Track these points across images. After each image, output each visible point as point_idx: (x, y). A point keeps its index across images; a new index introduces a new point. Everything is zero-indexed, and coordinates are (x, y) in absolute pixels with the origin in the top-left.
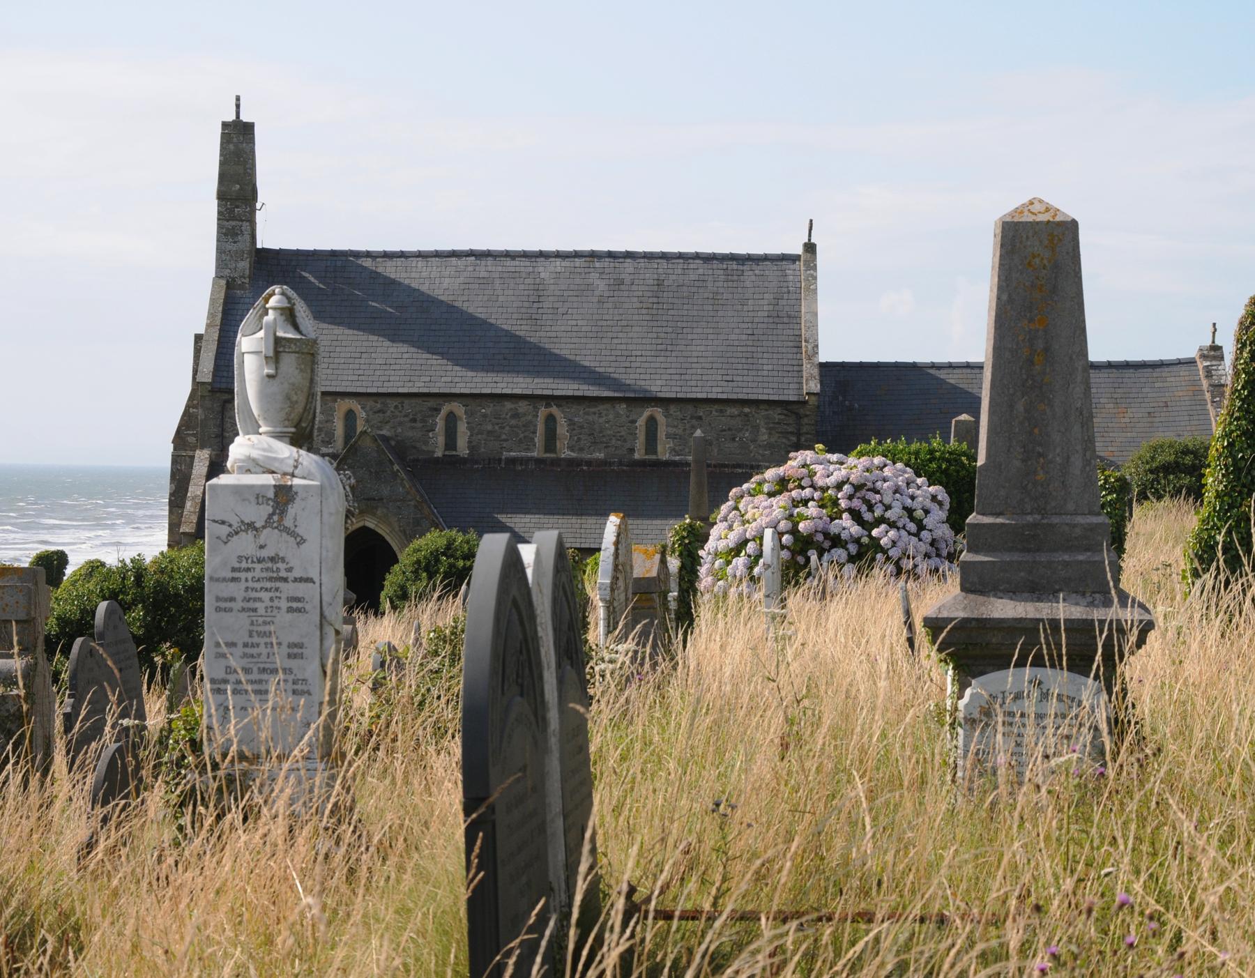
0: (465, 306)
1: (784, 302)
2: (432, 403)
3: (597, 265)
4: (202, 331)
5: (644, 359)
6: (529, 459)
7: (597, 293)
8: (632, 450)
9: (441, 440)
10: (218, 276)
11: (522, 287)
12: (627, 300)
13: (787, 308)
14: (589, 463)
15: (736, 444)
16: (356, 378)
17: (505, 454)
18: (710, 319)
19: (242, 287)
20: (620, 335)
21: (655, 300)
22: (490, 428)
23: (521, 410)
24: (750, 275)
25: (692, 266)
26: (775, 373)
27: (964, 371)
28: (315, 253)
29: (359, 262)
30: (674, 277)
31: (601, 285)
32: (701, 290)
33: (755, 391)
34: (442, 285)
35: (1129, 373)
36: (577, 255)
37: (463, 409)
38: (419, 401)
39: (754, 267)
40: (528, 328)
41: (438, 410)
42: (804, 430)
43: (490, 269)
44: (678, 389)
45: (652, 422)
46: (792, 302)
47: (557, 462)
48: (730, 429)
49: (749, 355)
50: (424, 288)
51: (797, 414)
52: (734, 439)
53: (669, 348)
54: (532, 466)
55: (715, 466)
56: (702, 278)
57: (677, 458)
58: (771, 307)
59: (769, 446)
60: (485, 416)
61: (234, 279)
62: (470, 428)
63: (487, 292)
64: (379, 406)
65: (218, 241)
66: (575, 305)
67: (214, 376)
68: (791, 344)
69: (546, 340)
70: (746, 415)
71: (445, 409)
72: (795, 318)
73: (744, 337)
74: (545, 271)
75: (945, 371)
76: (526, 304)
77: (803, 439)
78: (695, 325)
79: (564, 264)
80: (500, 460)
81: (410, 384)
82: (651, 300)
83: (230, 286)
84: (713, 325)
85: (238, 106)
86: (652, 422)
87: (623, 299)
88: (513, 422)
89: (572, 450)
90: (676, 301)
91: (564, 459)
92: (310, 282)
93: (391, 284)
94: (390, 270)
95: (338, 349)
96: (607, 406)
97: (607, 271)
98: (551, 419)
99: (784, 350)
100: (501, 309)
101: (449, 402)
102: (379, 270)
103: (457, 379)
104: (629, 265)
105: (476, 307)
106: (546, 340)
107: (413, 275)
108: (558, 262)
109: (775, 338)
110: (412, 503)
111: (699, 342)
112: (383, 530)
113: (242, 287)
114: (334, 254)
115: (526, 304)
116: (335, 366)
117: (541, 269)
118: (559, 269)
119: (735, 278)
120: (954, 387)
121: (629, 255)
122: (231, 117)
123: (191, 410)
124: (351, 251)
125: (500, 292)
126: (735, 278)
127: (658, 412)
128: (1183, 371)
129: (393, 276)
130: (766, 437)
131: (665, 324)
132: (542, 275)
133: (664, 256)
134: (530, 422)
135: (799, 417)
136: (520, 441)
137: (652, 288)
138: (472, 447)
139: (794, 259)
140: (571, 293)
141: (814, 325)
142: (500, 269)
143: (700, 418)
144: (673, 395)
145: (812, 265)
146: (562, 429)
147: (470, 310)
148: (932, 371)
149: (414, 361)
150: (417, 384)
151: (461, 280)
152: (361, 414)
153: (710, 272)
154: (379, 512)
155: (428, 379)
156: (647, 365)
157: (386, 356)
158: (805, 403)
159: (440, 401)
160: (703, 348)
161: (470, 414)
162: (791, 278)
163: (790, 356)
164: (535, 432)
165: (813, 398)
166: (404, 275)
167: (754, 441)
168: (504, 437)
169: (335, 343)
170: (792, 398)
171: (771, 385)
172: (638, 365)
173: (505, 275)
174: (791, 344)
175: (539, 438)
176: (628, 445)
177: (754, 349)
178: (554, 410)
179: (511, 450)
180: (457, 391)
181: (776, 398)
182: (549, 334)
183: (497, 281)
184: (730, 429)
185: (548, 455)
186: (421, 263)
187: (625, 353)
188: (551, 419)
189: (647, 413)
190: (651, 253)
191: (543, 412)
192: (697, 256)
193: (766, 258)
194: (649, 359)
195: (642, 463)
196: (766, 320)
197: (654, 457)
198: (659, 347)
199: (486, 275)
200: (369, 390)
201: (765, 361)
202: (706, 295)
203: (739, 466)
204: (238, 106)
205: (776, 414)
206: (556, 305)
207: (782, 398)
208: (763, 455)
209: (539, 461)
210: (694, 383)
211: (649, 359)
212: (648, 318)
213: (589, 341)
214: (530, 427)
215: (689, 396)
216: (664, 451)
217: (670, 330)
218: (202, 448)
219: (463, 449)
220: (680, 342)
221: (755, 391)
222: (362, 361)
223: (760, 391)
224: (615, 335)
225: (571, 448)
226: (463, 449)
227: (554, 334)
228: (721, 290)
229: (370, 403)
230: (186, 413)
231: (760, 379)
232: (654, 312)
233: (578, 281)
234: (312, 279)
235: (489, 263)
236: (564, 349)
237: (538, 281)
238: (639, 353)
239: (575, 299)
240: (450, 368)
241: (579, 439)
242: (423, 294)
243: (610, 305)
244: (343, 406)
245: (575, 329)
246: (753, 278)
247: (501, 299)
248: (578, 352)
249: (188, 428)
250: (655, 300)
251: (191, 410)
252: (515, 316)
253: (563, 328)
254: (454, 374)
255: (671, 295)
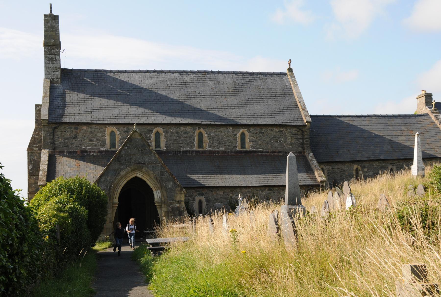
0: (156, 91)
1: (286, 89)
2: (149, 128)
3: (208, 76)
4: (40, 102)
5: (236, 110)
6: (192, 151)
7: (210, 86)
8: (235, 147)
9: (153, 144)
10: (46, 78)
11: (179, 83)
12: (223, 88)
13: (287, 92)
14: (218, 152)
15: (278, 143)
16: (114, 117)
17: (182, 149)
18: (258, 95)
19: (57, 82)
20: (224, 101)
21: (235, 88)
22: (175, 138)
23: (188, 131)
24: (270, 80)
25: (245, 76)
26: (291, 115)
27: (349, 118)
28: (88, 71)
29: (108, 74)
30: (240, 80)
31: (211, 83)
32: (252, 85)
33: (284, 121)
34: (146, 83)
35: (407, 118)
36: (199, 72)
37: (163, 130)
38: (143, 127)
39: (270, 77)
40: (185, 98)
41: (152, 131)
42: (305, 137)
43: (164, 77)
44: (254, 121)
45: (243, 135)
46: (289, 89)
47: (204, 152)
48: (275, 137)
49: (278, 108)
50: (137, 84)
51: (302, 131)
52: (277, 141)
53: (245, 106)
54: (194, 154)
55: (271, 153)
56: (251, 81)
57: (254, 150)
58: (281, 91)
59: (292, 144)
60: (172, 133)
61: (53, 79)
62: (166, 138)
63: (164, 85)
64: (125, 129)
65: (45, 63)
66: (202, 90)
67: (49, 117)
68: (294, 104)
69: (194, 103)
70: (282, 131)
71: (155, 130)
72: (291, 95)
73: (274, 102)
74: (187, 78)
75: (342, 118)
76: (182, 90)
77: (305, 141)
78: (253, 97)
79: (194, 75)
80: (180, 152)
81: (139, 120)
82: (233, 88)
83: (52, 82)
84: (260, 97)
85: (51, 8)
86: (243, 135)
87: (221, 88)
88: (185, 136)
89: (210, 147)
90: (243, 89)
91: (208, 151)
92: (87, 81)
93: (123, 83)
94: (121, 77)
95: (104, 106)
96: (224, 128)
97: (212, 78)
98: (200, 134)
99: (291, 106)
100: (173, 92)
101: (157, 127)
102: (117, 77)
103: (159, 118)
104: (221, 76)
105: (161, 91)
106: (194, 103)
107: (132, 79)
108: (192, 75)
109: (286, 102)
110: (160, 165)
111: (256, 104)
112: (145, 178)
113: (57, 82)
114: (96, 71)
115: (182, 90)
116: (104, 113)
117: (185, 77)
118: (192, 77)
119: (264, 81)
120: (348, 124)
121: (220, 72)
122: (48, 13)
123: (35, 136)
124: (104, 70)
125: (170, 85)
126: (264, 81)
127: (245, 131)
128: (426, 118)
129: (123, 79)
130: (290, 140)
131: (241, 97)
132: (186, 79)
133: (234, 73)
134: (192, 135)
135: (303, 132)
136: (188, 144)
137: (232, 84)
138: (167, 146)
139: (285, 74)
140: (200, 86)
141: (300, 97)
142: (168, 77)
143: (263, 133)
144: (252, 123)
145: (293, 76)
146: (206, 138)
147: (159, 92)
148: (338, 118)
149: (139, 111)
150: (142, 120)
151: (153, 81)
152: (117, 132)
153: (254, 79)
154: (144, 169)
155: (146, 118)
156: (238, 112)
157: (126, 109)
158: (306, 126)
159: (152, 127)
160: (259, 106)
161: (166, 132)
162: (286, 81)
163: (294, 109)
164: (194, 140)
165: (309, 124)
166: (127, 79)
167: (285, 142)
168: (181, 142)
169: (102, 104)
170: (300, 124)
171: (290, 119)
172: (234, 112)
173: (171, 79)
174: (294, 104)
175: (196, 142)
176: (234, 145)
177: (279, 106)
178: (202, 130)
179: (184, 148)
180: (160, 122)
181: (294, 124)
182: (194, 101)
183: (168, 81)
184: (275, 137)
185: (200, 149)
186: (134, 75)
187: (228, 108)
188: (200, 134)
189: (241, 131)
190: (229, 72)
191: (197, 131)
192: (247, 73)
193: (274, 74)
194: (238, 110)
195: (240, 152)
196: (281, 96)
197: (244, 149)
198: (241, 105)
199: (163, 79)
200: (121, 122)
201: (285, 111)
202: (254, 87)
203: (280, 152)
204: (51, 8)
205: (294, 131)
206: (194, 90)
207: (296, 124)
208: (289, 148)
209: (197, 152)
210: (259, 119)
211: (238, 110)
212: (233, 95)
213: (211, 103)
214: (192, 137)
215: (259, 123)
216: (248, 147)
217: (244, 99)
218: (44, 149)
219: (163, 147)
220: (249, 103)
221: (284, 121)
222: (116, 111)
223: (287, 121)
224: (222, 101)
225: (210, 146)
226: (163, 147)
227: (196, 101)
228: (260, 85)
229: (121, 128)
230: (33, 137)
231: (285, 117)
232: (235, 93)
233: (201, 81)
234: (88, 80)
235: (163, 75)
236: (202, 106)
237: (185, 81)
238: (234, 108)
239: (202, 88)
240: (155, 113)
241: (213, 142)
242: (137, 86)
243: (217, 90)
244: (109, 129)
245: (204, 99)
246: (271, 81)
247: (171, 88)
248: (208, 107)
249: (34, 144)
250: (235, 88)
251: (35, 136)
252: (178, 94)
253: (199, 99)
254: (157, 116)
255: (240, 86)
